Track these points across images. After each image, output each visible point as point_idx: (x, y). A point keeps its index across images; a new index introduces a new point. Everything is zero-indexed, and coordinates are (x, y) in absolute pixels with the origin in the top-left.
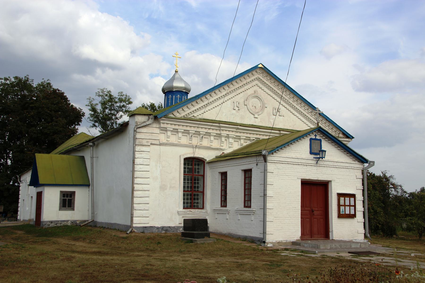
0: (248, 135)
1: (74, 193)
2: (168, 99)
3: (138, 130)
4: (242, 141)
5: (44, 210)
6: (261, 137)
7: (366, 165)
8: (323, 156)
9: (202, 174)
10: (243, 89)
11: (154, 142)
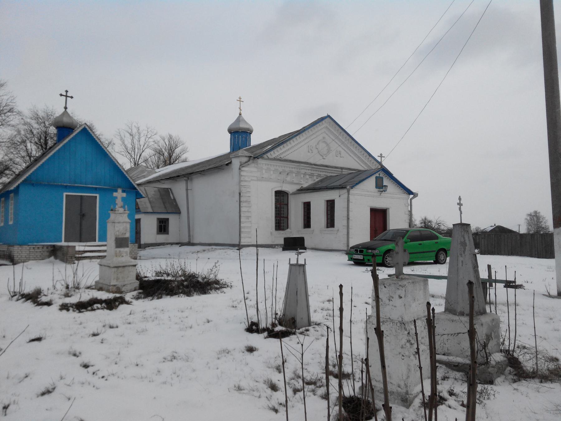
0: (320, 173)
1: (168, 219)
2: (235, 137)
3: (243, 169)
4: (315, 177)
5: (390, 215)
6: (329, 175)
7: (411, 196)
8: (386, 190)
9: (287, 203)
10: (315, 136)
11: (253, 178)
